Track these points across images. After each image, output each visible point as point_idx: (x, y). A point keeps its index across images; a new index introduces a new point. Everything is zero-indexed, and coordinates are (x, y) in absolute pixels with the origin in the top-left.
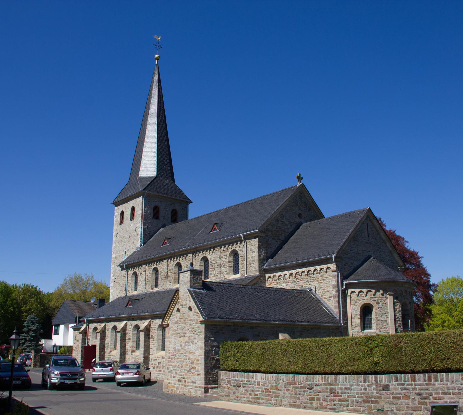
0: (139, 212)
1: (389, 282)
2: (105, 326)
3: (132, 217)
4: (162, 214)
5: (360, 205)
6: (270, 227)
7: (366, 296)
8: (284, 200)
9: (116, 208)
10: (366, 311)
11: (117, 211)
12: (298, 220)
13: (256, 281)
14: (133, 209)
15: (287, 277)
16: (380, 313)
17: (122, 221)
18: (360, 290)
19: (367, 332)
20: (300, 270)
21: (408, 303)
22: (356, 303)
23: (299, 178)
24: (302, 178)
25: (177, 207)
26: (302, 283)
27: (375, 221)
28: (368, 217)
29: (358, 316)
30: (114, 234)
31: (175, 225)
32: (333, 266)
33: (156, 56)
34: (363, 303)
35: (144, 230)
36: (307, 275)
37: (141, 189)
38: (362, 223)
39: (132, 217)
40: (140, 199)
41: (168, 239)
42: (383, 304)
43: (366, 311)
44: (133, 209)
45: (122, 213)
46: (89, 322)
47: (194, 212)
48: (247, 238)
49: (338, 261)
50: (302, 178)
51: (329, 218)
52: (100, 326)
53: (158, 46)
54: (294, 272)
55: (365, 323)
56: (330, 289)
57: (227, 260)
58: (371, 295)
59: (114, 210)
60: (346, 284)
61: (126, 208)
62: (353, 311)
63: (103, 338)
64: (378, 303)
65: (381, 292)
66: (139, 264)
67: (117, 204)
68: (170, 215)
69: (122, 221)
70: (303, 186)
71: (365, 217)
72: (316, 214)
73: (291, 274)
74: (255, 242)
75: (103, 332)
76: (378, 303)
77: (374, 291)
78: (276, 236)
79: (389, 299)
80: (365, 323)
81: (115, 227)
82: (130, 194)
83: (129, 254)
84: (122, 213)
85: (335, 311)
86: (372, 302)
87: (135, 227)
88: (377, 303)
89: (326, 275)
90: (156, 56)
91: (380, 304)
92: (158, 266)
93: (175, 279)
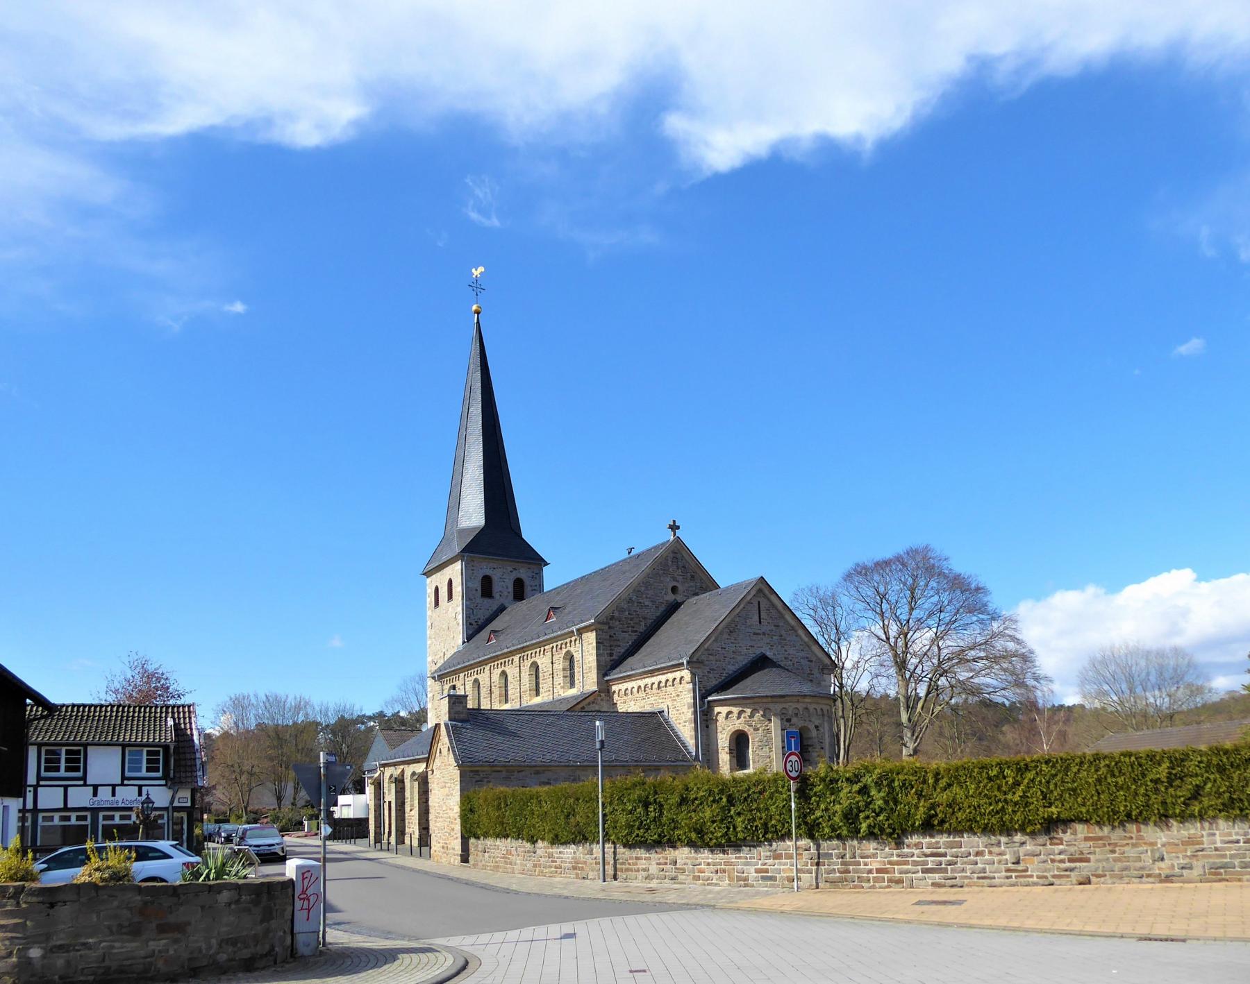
0: (458, 589)
1: (772, 697)
2: (403, 771)
3: (450, 597)
4: (497, 588)
5: (751, 575)
6: (616, 614)
7: (739, 718)
8: (645, 566)
9: (429, 580)
10: (740, 742)
11: (432, 582)
12: (670, 597)
13: (591, 699)
14: (450, 582)
15: (635, 690)
17: (437, 604)
19: (740, 774)
20: (648, 681)
21: (812, 727)
23: (674, 527)
24: (678, 528)
25: (523, 573)
26: (652, 700)
27: (773, 597)
28: (760, 591)
29: (727, 750)
30: (429, 624)
31: (519, 604)
32: (686, 674)
33: (474, 307)
35: (468, 617)
36: (659, 687)
37: (457, 550)
38: (745, 603)
39: (450, 597)
40: (457, 567)
41: (554, 609)
43: (740, 742)
44: (450, 582)
45: (437, 589)
46: (384, 766)
47: (552, 578)
48: (580, 632)
49: (693, 664)
50: (678, 528)
51: (727, 589)
52: (396, 771)
53: (477, 286)
54: (642, 683)
55: (740, 759)
56: (685, 709)
57: (561, 667)
59: (425, 585)
61: (440, 579)
62: (723, 740)
63: (400, 792)
64: (756, 729)
66: (456, 672)
67: (428, 574)
68: (511, 589)
69: (437, 604)
70: (678, 540)
71: (753, 592)
72: (704, 583)
73: (639, 687)
74: (591, 638)
75: (399, 782)
76: (756, 729)
77: (749, 711)
79: (775, 725)
80: (740, 759)
81: (429, 613)
82: (445, 558)
83: (448, 655)
84: (437, 589)
85: (690, 742)
86: (746, 729)
87: (453, 614)
89: (680, 688)
90: (477, 272)
92: (479, 677)
93: (500, 696)
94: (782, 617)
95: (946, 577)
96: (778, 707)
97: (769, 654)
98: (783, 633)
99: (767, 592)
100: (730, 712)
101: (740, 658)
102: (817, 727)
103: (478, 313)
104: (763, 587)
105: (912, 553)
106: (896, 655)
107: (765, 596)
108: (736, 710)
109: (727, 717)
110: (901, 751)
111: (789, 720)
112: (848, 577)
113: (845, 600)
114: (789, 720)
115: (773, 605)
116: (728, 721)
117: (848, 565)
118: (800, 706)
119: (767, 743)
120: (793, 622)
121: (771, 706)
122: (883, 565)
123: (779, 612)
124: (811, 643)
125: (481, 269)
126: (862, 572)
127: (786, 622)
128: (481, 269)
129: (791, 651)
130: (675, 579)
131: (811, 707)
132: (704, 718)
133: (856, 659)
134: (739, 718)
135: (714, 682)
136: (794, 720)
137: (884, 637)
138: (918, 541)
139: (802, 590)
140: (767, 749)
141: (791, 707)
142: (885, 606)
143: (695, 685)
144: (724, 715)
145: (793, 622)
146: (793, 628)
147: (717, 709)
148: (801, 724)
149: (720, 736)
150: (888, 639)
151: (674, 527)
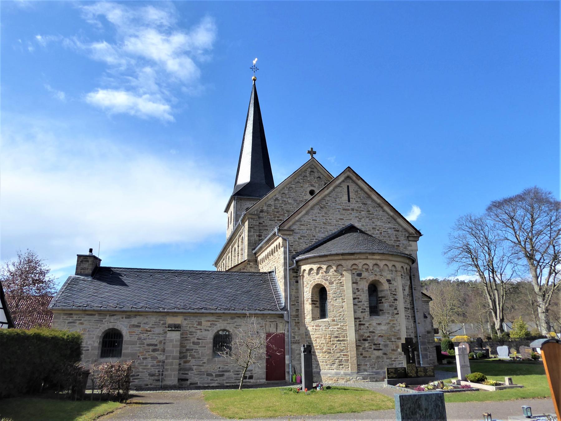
1: (343, 254)
6: (265, 208)
7: (317, 273)
10: (321, 293)
16: (334, 295)
18: (319, 266)
21: (383, 280)
22: (308, 284)
23: (312, 152)
27: (360, 182)
29: (310, 301)
33: (253, 78)
34: (314, 284)
42: (337, 283)
43: (321, 293)
50: (315, 153)
53: (254, 68)
58: (322, 273)
60: (297, 262)
62: (307, 294)
64: (331, 283)
65: (335, 268)
77: (324, 267)
78: (275, 217)
79: (347, 279)
88: (329, 283)
91: (334, 285)
94: (369, 197)
95: (551, 203)
96: (349, 263)
97: (357, 225)
98: (370, 209)
99: (354, 178)
100: (311, 269)
101: (329, 228)
102: (389, 281)
103: (255, 80)
104: (351, 175)
105: (527, 192)
106: (526, 251)
107: (354, 182)
108: (315, 267)
109: (309, 274)
110: (537, 310)
111: (359, 275)
112: (489, 209)
113: (490, 222)
114: (359, 275)
115: (362, 189)
116: (311, 276)
117: (488, 203)
118: (370, 263)
119: (340, 295)
120: (378, 201)
121: (343, 262)
122: (508, 201)
123: (366, 193)
124: (396, 217)
125: (256, 59)
126: (498, 205)
127: (373, 200)
128: (256, 59)
129: (379, 223)
130: (312, 185)
131: (382, 264)
132: (294, 274)
133: (502, 254)
134: (317, 273)
135: (304, 246)
136: (365, 274)
137: (517, 242)
138: (530, 185)
139: (462, 218)
140: (340, 300)
141: (360, 263)
142: (515, 223)
143: (285, 248)
144: (307, 272)
145: (378, 201)
146: (379, 205)
147: (303, 267)
148: (372, 278)
149: (306, 289)
150: (520, 242)
151: (312, 152)
